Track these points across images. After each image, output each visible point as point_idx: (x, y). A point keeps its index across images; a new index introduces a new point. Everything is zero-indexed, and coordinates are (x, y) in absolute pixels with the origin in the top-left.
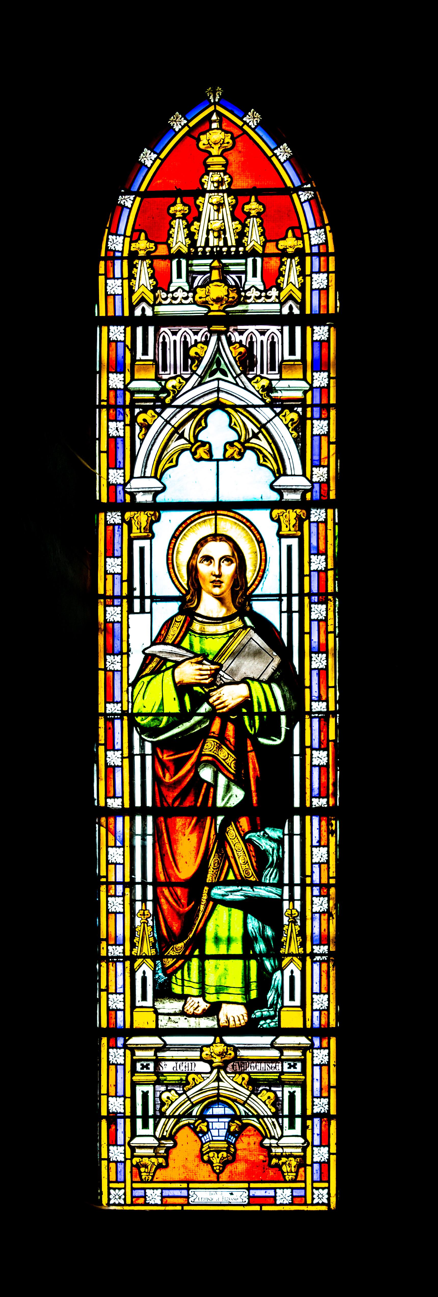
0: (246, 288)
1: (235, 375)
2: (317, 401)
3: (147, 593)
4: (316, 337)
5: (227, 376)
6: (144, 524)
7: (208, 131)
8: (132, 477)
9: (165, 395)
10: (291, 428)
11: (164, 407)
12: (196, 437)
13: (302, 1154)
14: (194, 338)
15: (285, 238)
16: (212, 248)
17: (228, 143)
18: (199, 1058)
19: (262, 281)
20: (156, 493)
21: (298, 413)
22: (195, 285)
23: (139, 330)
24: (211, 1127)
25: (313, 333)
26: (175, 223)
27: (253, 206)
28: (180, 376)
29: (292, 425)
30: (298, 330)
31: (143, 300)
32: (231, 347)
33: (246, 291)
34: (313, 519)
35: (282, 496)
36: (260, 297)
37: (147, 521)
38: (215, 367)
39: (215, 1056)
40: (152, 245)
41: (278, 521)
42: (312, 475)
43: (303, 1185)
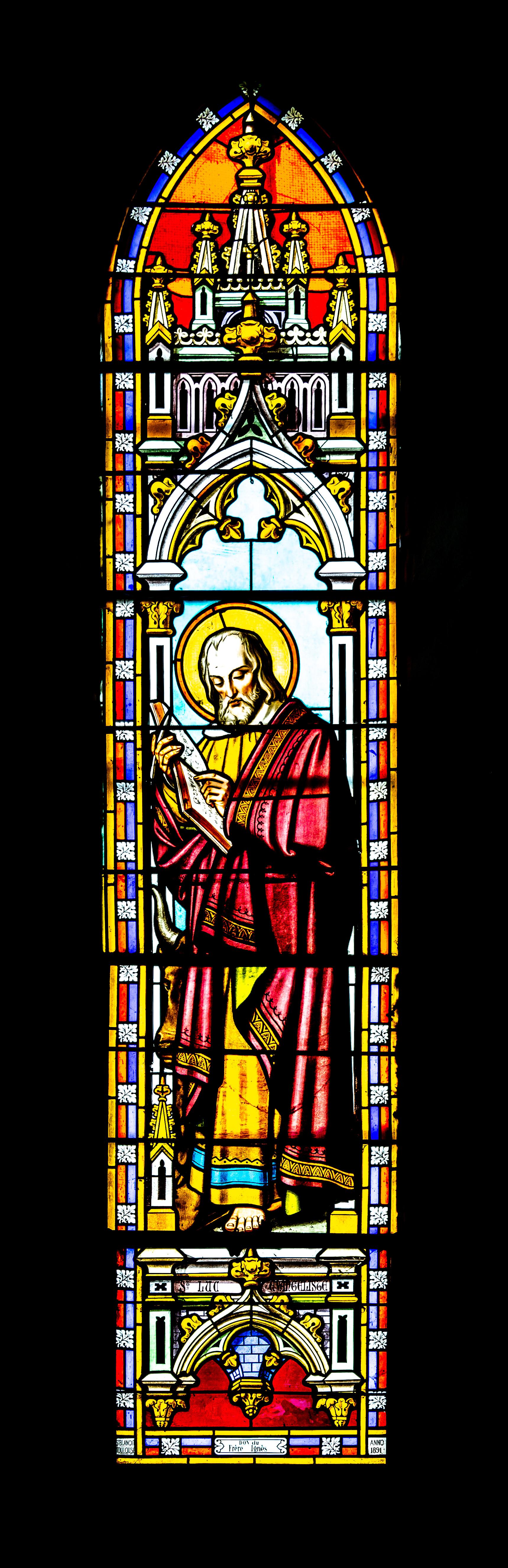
0: (287, 326)
2: (373, 463)
6: (163, 617)
7: (241, 136)
8: (145, 560)
9: (185, 458)
11: (186, 473)
12: (224, 510)
13: (356, 1299)
14: (220, 385)
19: (307, 318)
21: (350, 481)
22: (224, 323)
24: (242, 1361)
31: (159, 339)
33: (286, 331)
35: (330, 586)
38: (246, 423)
39: (246, 1273)
41: (328, 614)
42: (367, 561)
43: (355, 1432)
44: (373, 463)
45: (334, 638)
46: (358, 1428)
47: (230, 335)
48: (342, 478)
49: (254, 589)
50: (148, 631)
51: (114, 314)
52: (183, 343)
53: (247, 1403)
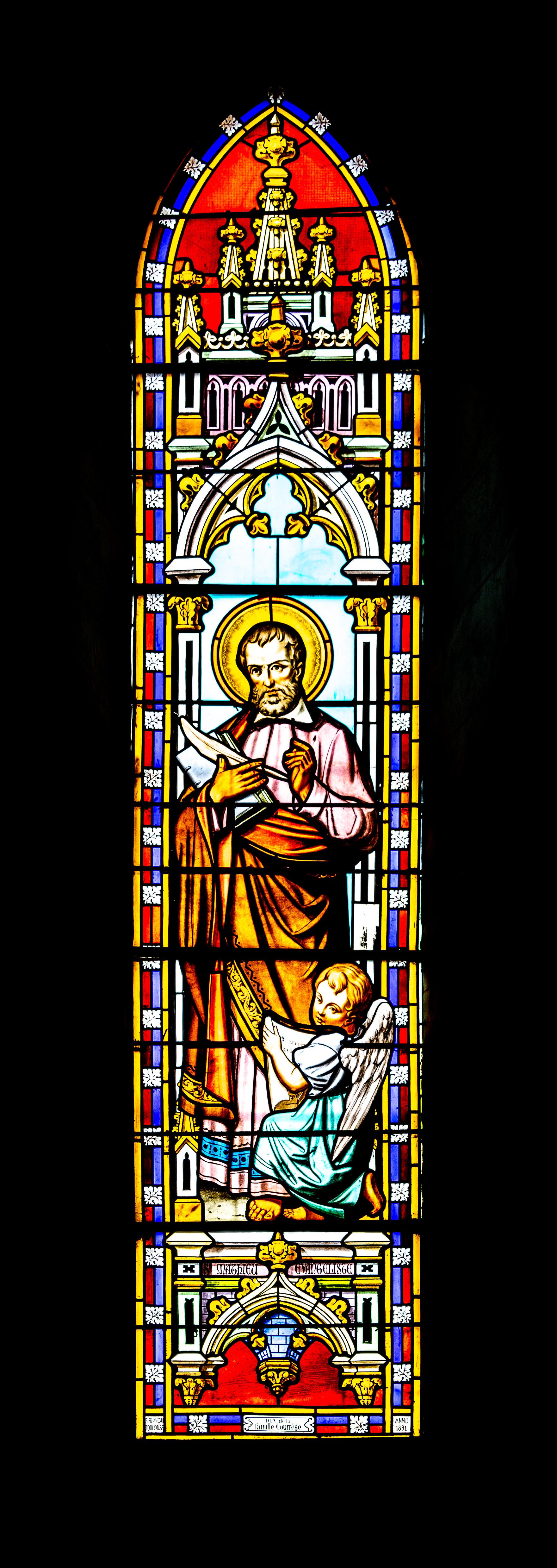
3: (195, 697)
4: (397, 387)
7: (267, 137)
8: (174, 556)
12: (252, 507)
14: (249, 387)
16: (271, 282)
18: (254, 1258)
19: (332, 321)
20: (204, 576)
21: (375, 478)
23: (182, 379)
25: (393, 382)
26: (227, 250)
27: (321, 230)
28: (232, 432)
29: (367, 493)
30: (375, 378)
31: (188, 344)
32: (294, 398)
33: (312, 334)
34: (395, 609)
35: (355, 582)
38: (274, 422)
41: (353, 613)
43: (380, 1411)
46: (383, 1407)
47: (257, 338)
48: (367, 475)
49: (281, 583)
50: (177, 627)
52: (212, 347)
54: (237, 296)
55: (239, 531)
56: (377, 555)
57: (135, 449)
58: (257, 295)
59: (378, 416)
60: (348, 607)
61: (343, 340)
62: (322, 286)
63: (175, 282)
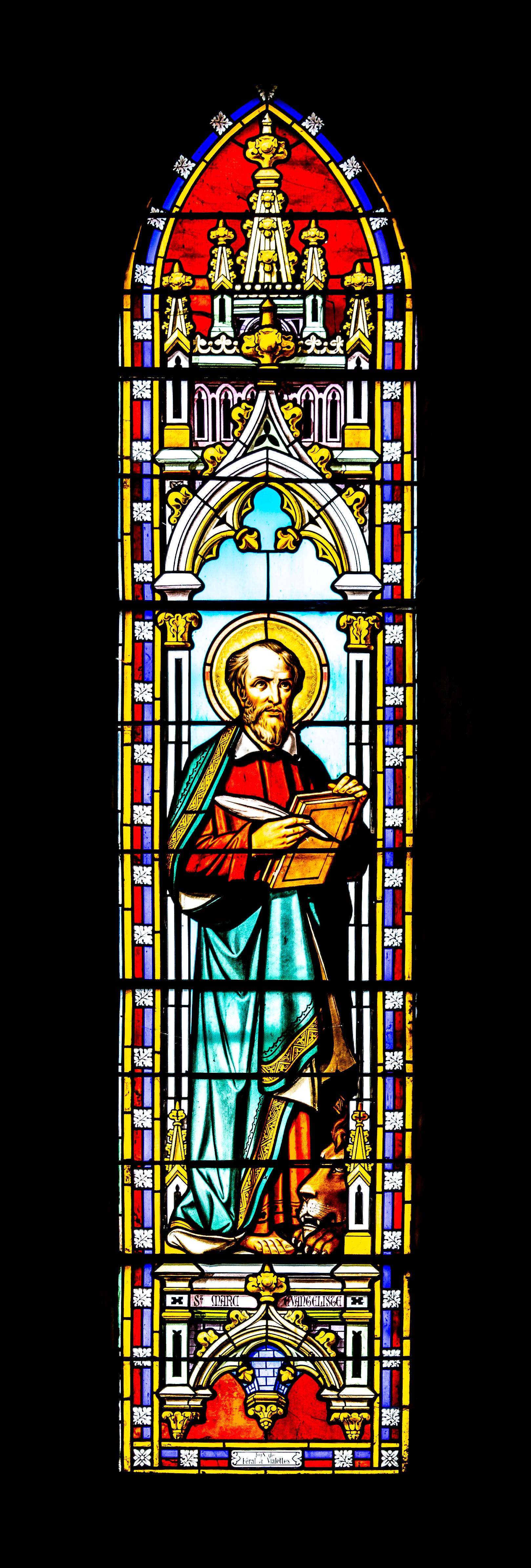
0: (305, 335)
1: (287, 444)
3: (185, 718)
5: (278, 445)
7: (257, 137)
10: (356, 511)
12: (241, 522)
14: (237, 395)
15: (352, 272)
16: (263, 285)
17: (282, 153)
19: (324, 326)
21: (365, 492)
22: (242, 332)
26: (217, 251)
27: (313, 233)
28: (220, 443)
31: (177, 347)
32: (282, 408)
36: (320, 348)
37: (185, 627)
40: (189, 278)
41: (347, 631)
42: (383, 574)
43: (368, 1445)
44: (388, 476)
45: (351, 654)
48: (357, 489)
49: (271, 598)
51: (133, 319)
52: (202, 351)
53: (261, 1416)
54: (228, 299)
55: (229, 546)
56: (368, 570)
57: (123, 458)
58: (248, 298)
59: (367, 427)
60: (341, 624)
61: (335, 347)
62: (314, 291)
63: (164, 284)
